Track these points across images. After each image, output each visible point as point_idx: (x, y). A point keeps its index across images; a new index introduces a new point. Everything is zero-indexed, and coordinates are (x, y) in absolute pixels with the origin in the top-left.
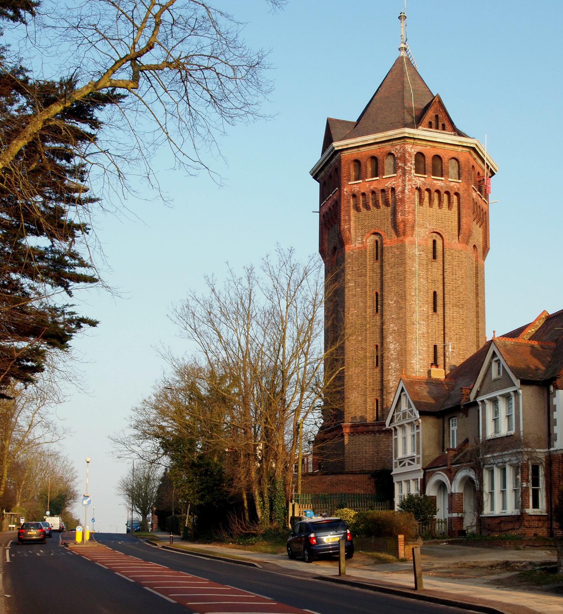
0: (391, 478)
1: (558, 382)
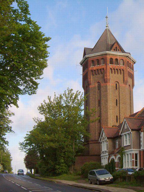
0: (101, 157)
1: (142, 130)
